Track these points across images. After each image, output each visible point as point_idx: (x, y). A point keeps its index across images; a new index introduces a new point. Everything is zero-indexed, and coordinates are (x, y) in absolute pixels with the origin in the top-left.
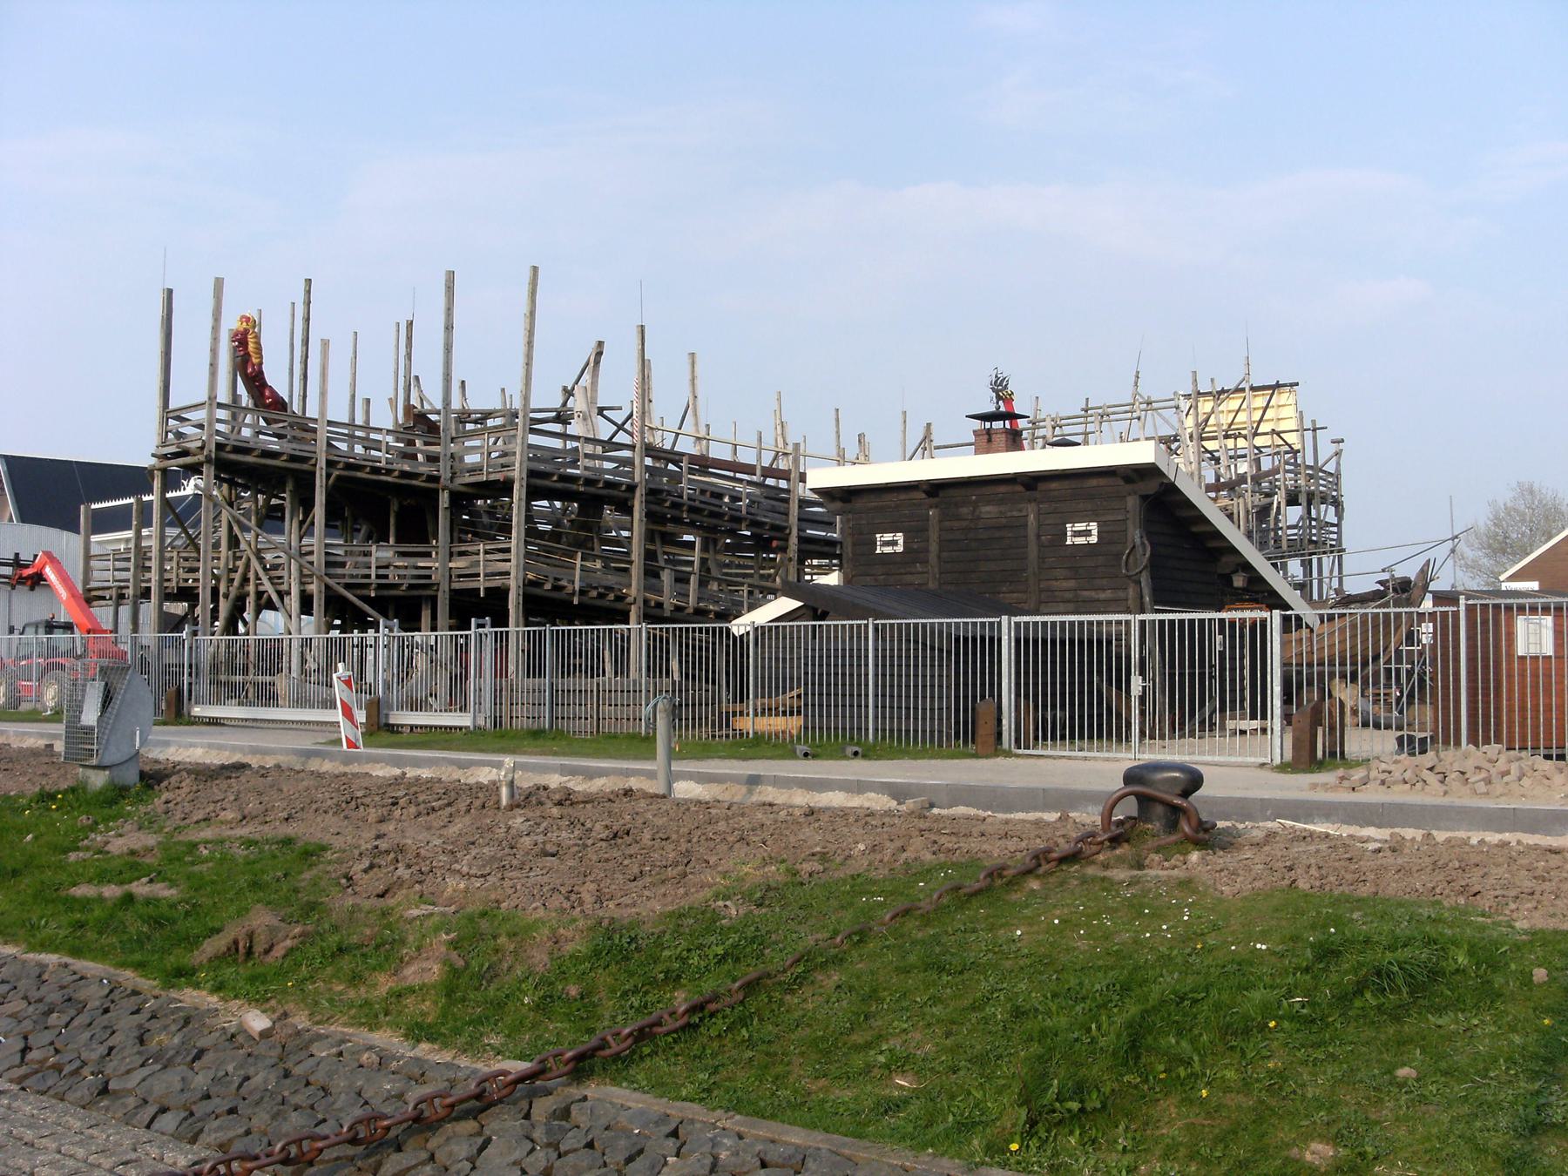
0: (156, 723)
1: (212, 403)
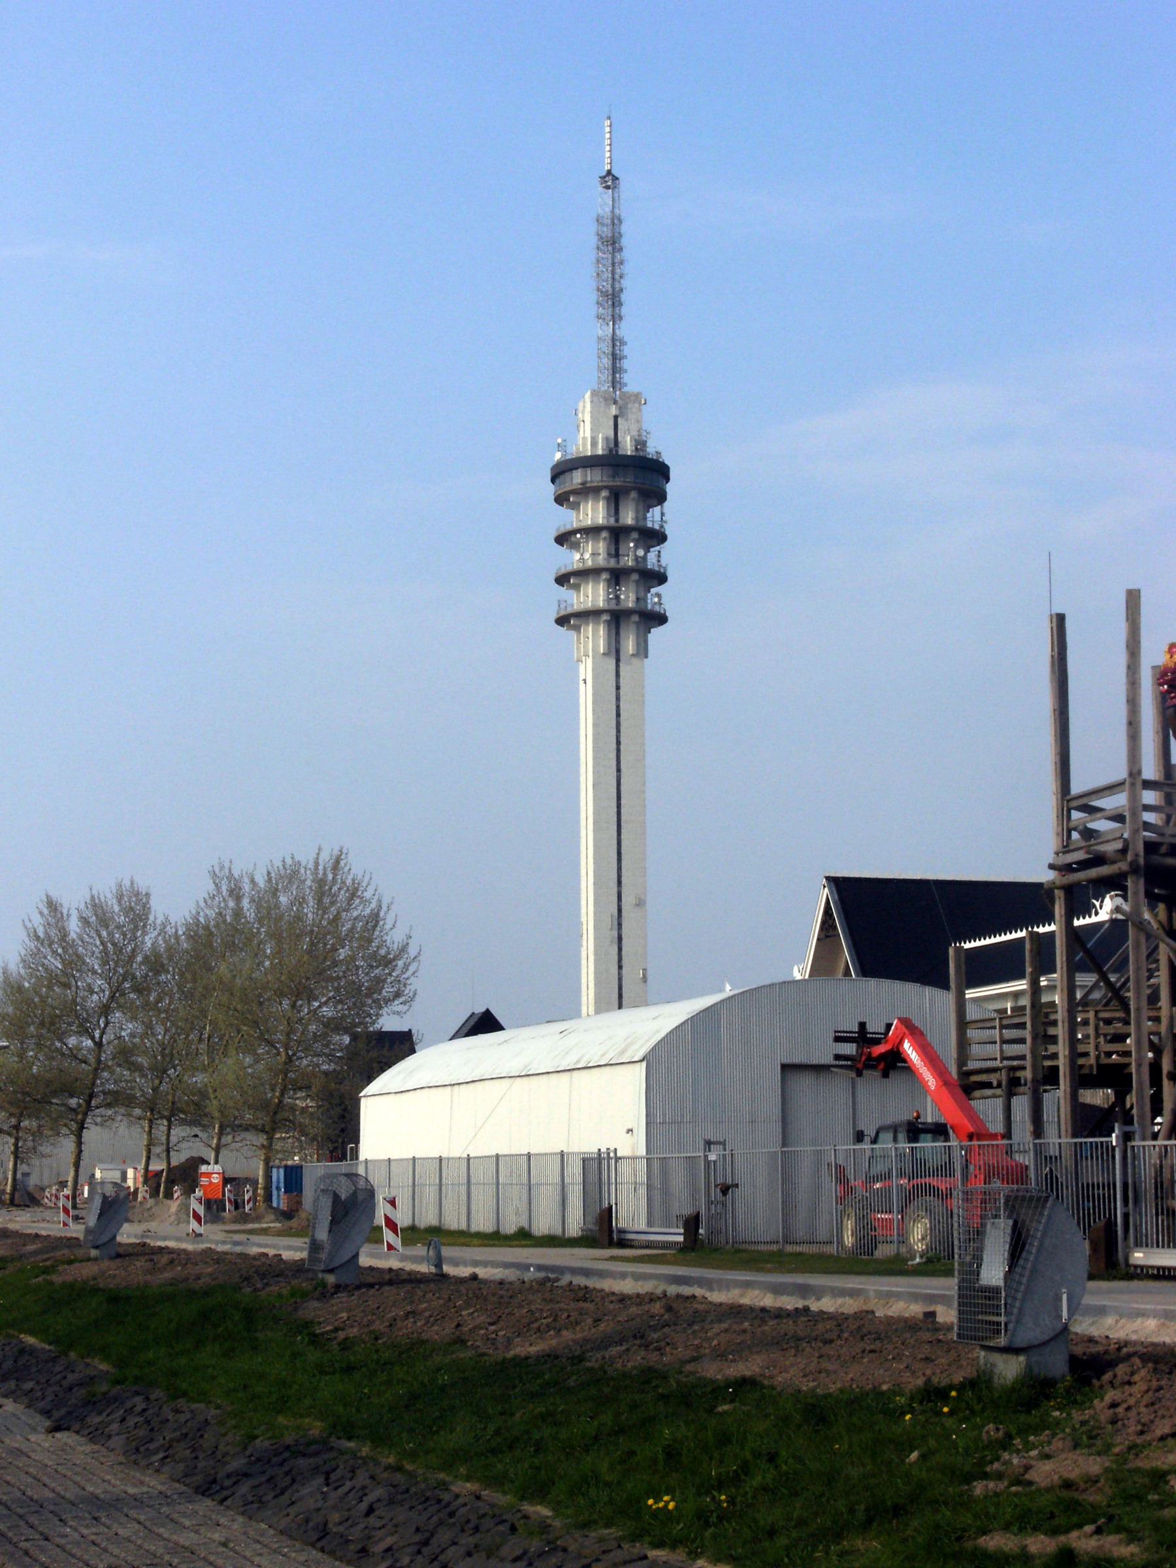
0: (1091, 1277)
1: (1135, 781)
